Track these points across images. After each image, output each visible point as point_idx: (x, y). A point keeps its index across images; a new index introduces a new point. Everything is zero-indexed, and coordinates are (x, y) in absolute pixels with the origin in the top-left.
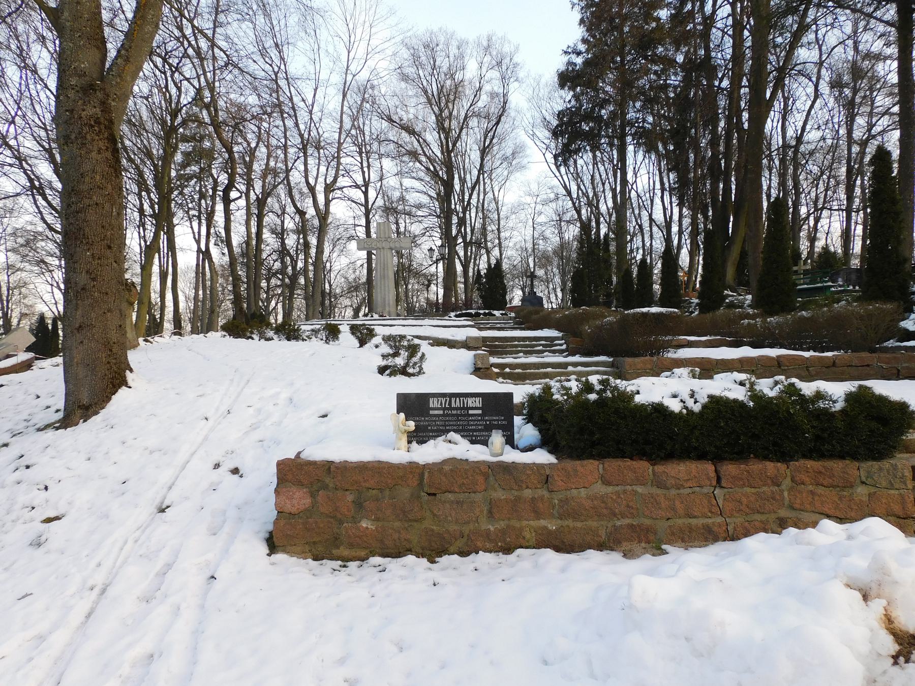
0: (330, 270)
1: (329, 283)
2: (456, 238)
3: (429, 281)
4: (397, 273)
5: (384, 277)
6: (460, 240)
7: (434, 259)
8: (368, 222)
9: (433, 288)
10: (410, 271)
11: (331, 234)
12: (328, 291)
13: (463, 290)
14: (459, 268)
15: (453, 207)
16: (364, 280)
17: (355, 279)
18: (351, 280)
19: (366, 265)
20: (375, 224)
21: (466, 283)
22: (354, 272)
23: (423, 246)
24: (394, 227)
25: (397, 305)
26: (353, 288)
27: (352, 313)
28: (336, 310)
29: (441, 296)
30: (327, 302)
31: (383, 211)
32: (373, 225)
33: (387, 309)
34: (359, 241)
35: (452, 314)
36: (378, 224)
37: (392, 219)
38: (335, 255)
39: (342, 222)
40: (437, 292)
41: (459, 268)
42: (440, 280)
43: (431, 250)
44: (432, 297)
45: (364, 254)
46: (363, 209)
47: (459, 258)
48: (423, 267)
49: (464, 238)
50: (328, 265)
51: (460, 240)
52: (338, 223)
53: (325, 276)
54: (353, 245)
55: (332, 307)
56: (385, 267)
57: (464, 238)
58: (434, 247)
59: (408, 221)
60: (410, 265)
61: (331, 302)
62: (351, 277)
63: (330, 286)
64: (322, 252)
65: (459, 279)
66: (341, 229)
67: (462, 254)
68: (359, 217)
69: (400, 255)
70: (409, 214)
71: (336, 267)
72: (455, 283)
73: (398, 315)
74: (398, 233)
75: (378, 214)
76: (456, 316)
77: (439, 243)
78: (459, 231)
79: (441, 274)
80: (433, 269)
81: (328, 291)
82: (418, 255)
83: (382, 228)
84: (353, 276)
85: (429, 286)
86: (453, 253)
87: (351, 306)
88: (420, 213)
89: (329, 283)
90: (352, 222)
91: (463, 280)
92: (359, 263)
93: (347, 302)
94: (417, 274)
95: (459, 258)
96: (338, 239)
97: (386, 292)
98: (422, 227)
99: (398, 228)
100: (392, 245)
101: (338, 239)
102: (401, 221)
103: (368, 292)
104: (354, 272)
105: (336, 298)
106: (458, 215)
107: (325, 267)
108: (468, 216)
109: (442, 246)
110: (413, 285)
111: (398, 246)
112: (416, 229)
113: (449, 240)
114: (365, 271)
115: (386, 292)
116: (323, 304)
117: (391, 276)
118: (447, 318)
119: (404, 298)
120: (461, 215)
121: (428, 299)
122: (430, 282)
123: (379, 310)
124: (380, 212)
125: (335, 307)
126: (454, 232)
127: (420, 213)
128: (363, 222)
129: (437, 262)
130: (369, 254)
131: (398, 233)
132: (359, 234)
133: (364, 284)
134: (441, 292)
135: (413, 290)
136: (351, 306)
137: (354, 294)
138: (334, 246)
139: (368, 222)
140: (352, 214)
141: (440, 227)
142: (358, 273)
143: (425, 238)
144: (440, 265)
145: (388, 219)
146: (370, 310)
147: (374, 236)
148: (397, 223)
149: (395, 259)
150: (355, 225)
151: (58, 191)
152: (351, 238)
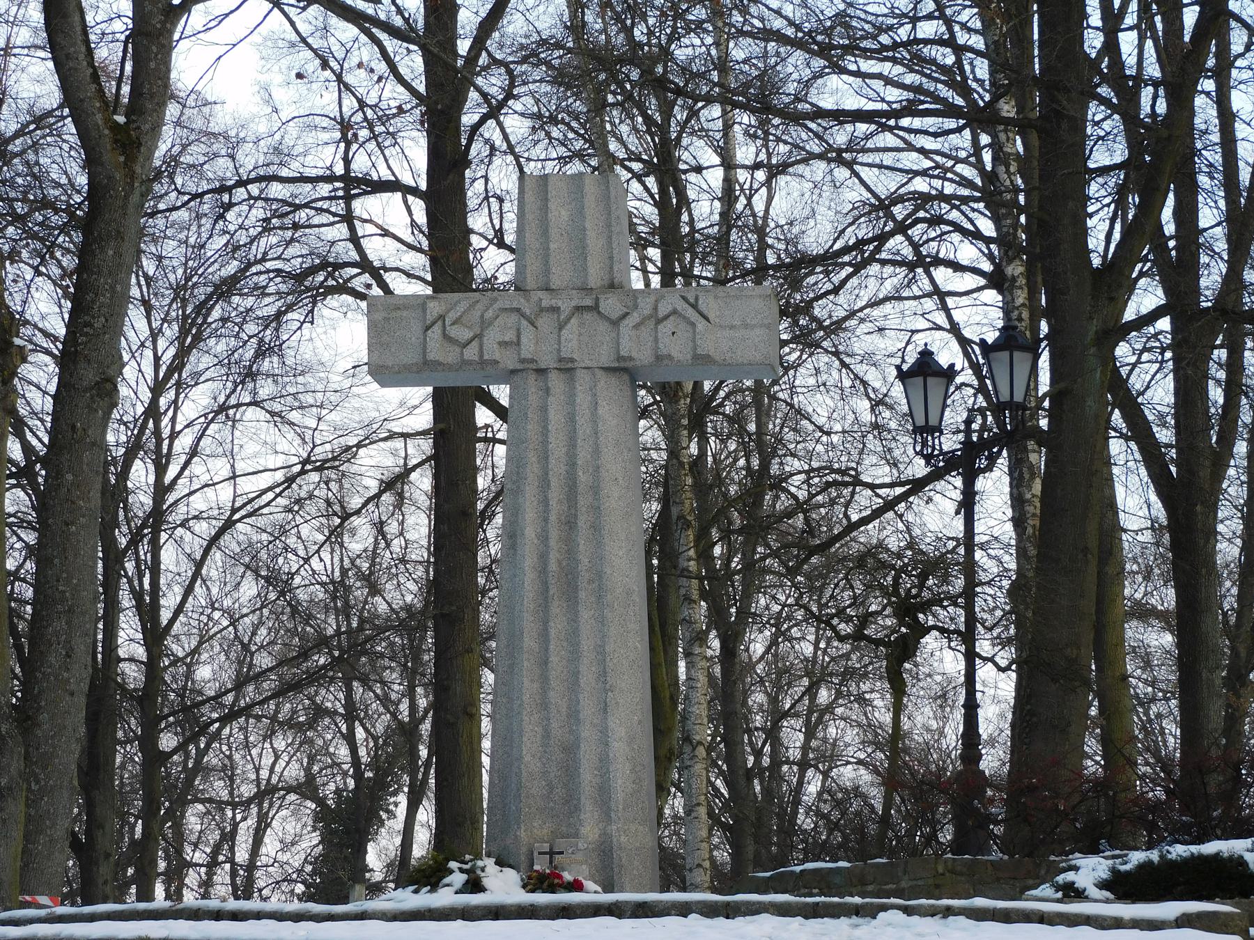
0: (157, 517)
1: (148, 611)
2: (1114, 280)
3: (916, 593)
4: (661, 539)
5: (568, 583)
6: (1147, 296)
7: (950, 442)
8: (448, 162)
9: (940, 658)
10: (757, 528)
11: (170, 247)
12: (132, 675)
13: (1168, 674)
14: (1136, 502)
15: (1093, 41)
16: (405, 591)
17: (338, 588)
18: (308, 592)
19: (422, 481)
20: (503, 177)
21: (1188, 620)
22: (335, 536)
23: (861, 340)
24: (641, 204)
25: (662, 790)
26: (322, 651)
27: (311, 841)
28: (193, 819)
29: (995, 716)
30: (126, 758)
31: (560, 78)
32: (493, 181)
33: (590, 830)
34: (386, 319)
35: (1090, 870)
36: (535, 190)
37: (626, 136)
38: (196, 402)
39: (249, 160)
40: (968, 692)
41: (1136, 502)
42: (992, 599)
43: (924, 371)
44: (931, 726)
45: (413, 407)
46: (413, 63)
47: (1140, 431)
48: (865, 501)
49: (1179, 276)
50: (141, 474)
51: (1147, 296)
52: (222, 168)
53: (114, 559)
54: (337, 336)
55: (165, 793)
56: (575, 511)
57: (1179, 276)
58: (948, 354)
59: (745, 153)
60: (763, 481)
61: (154, 758)
62: (314, 567)
63: (154, 635)
64: (106, 391)
65: (1133, 590)
66: (245, 216)
67: (1160, 394)
68: (379, 126)
69: (684, 408)
70: (762, 100)
71: (205, 490)
72: (1104, 618)
73: (671, 871)
74: (671, 235)
75: (523, 103)
76: (1122, 886)
77: (983, 316)
78: (1140, 231)
79: (998, 560)
80: (936, 516)
81: (132, 675)
82: (820, 407)
83: (560, 214)
84: (325, 563)
85: (902, 650)
86: (1090, 389)
87: (307, 788)
88: (837, 92)
89: (148, 611)
90: (323, 155)
91: (1167, 598)
92: (374, 463)
93: (277, 758)
94: (815, 550)
95: (1140, 431)
96: (225, 289)
97: (576, 688)
98: (854, 194)
99: (672, 200)
100: (635, 345)
101: (225, 289)
102: (699, 151)
103: (441, 689)
104: (335, 536)
105: (195, 729)
106: (1127, 107)
107: (118, 493)
108: (1205, 111)
109: (1012, 340)
110: (782, 632)
111: (676, 346)
112: (808, 207)
113: (1058, 291)
114: (418, 527)
115: (576, 688)
116: (95, 768)
117: (625, 569)
118: (1043, 898)
119: (705, 733)
120: (1152, 103)
121: (895, 740)
122: (909, 610)
123: (533, 832)
124: (536, 91)
125: (184, 795)
126: (1101, 233)
127: (837, 92)
128: (412, 156)
129: (968, 463)
130: (453, 410)
131: (671, 235)
132: (378, 250)
133: (408, 622)
134: (999, 689)
135: (781, 675)
136: (307, 788)
137: (332, 698)
138: (192, 335)
139: (448, 162)
140: (326, 100)
141: (992, 194)
142: (360, 539)
143: (879, 280)
144: (995, 486)
145: (597, 141)
146: (455, 835)
147: (492, 263)
148: (666, 169)
149: (650, 433)
150: (355, 185)
151: (142, 662)
152: (315, 282)
